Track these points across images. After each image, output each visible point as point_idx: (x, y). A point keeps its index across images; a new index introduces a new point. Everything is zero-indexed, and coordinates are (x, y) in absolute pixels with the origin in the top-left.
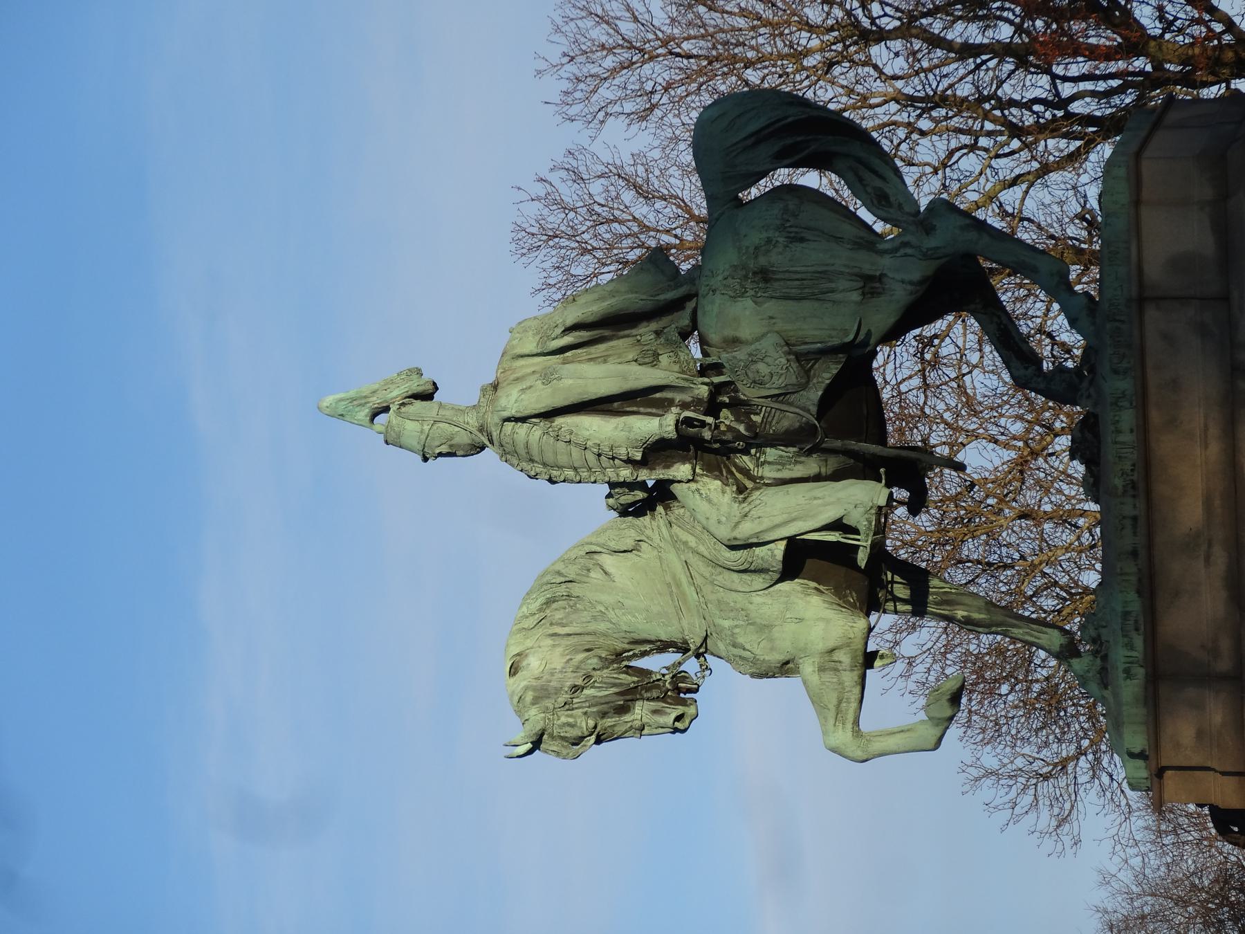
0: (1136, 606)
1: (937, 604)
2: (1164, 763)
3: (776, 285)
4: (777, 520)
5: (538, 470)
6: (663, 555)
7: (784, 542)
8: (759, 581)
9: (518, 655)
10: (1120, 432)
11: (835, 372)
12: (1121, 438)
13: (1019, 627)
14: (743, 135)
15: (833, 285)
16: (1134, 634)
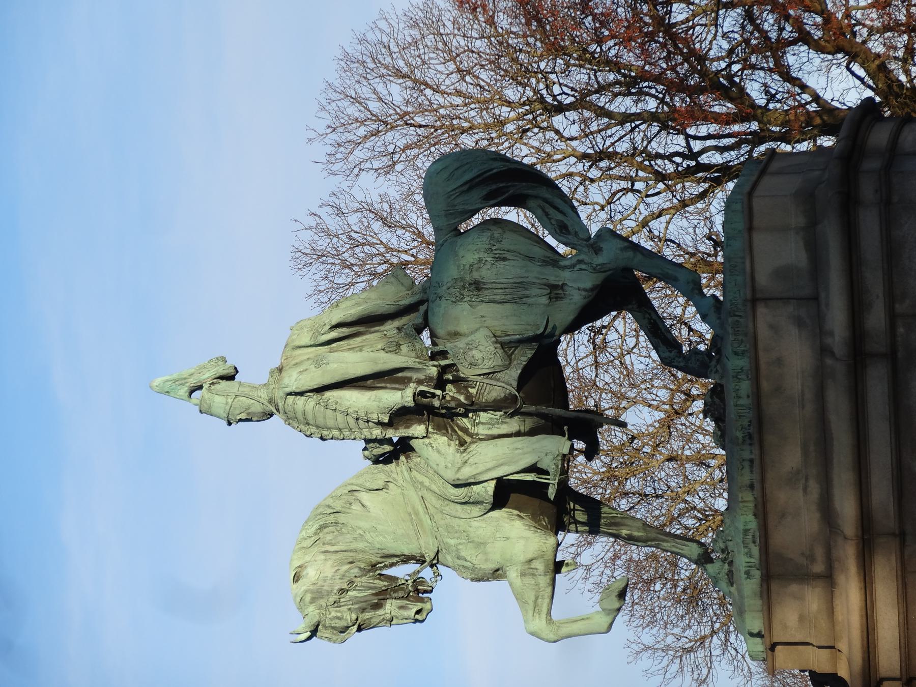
0: (753, 524)
1: (607, 525)
5: (313, 431)
6: (405, 492)
7: (494, 482)
8: (476, 510)
9: (299, 567)
11: (530, 356)
12: (741, 402)
13: (667, 542)
15: (527, 292)
16: (752, 545)
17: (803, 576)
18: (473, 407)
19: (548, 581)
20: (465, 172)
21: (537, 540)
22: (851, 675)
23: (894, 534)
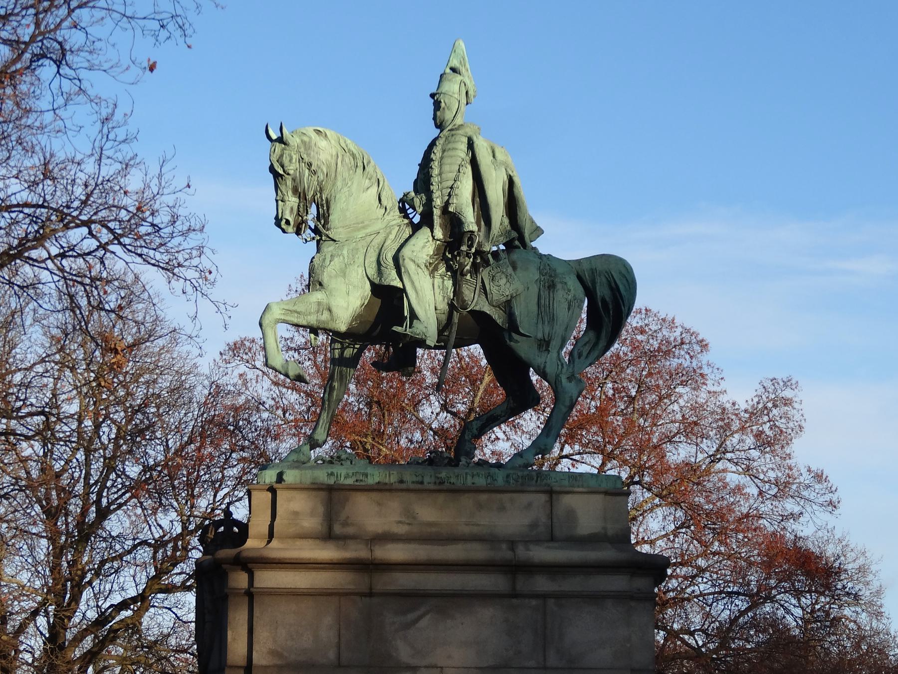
0: (371, 481)
1: (341, 372)
2: (279, 493)
3: (547, 293)
4: (417, 284)
5: (438, 154)
6: (380, 221)
7: (402, 287)
8: (372, 271)
9: (326, 135)
10: (473, 477)
11: (498, 322)
12: (469, 478)
13: (327, 417)
14: (618, 282)
15: (546, 322)
16: (354, 479)
17: (330, 517)
18: (456, 275)
19: (312, 323)
20: (624, 286)
21: (345, 317)
22: (248, 549)
23: (371, 589)
